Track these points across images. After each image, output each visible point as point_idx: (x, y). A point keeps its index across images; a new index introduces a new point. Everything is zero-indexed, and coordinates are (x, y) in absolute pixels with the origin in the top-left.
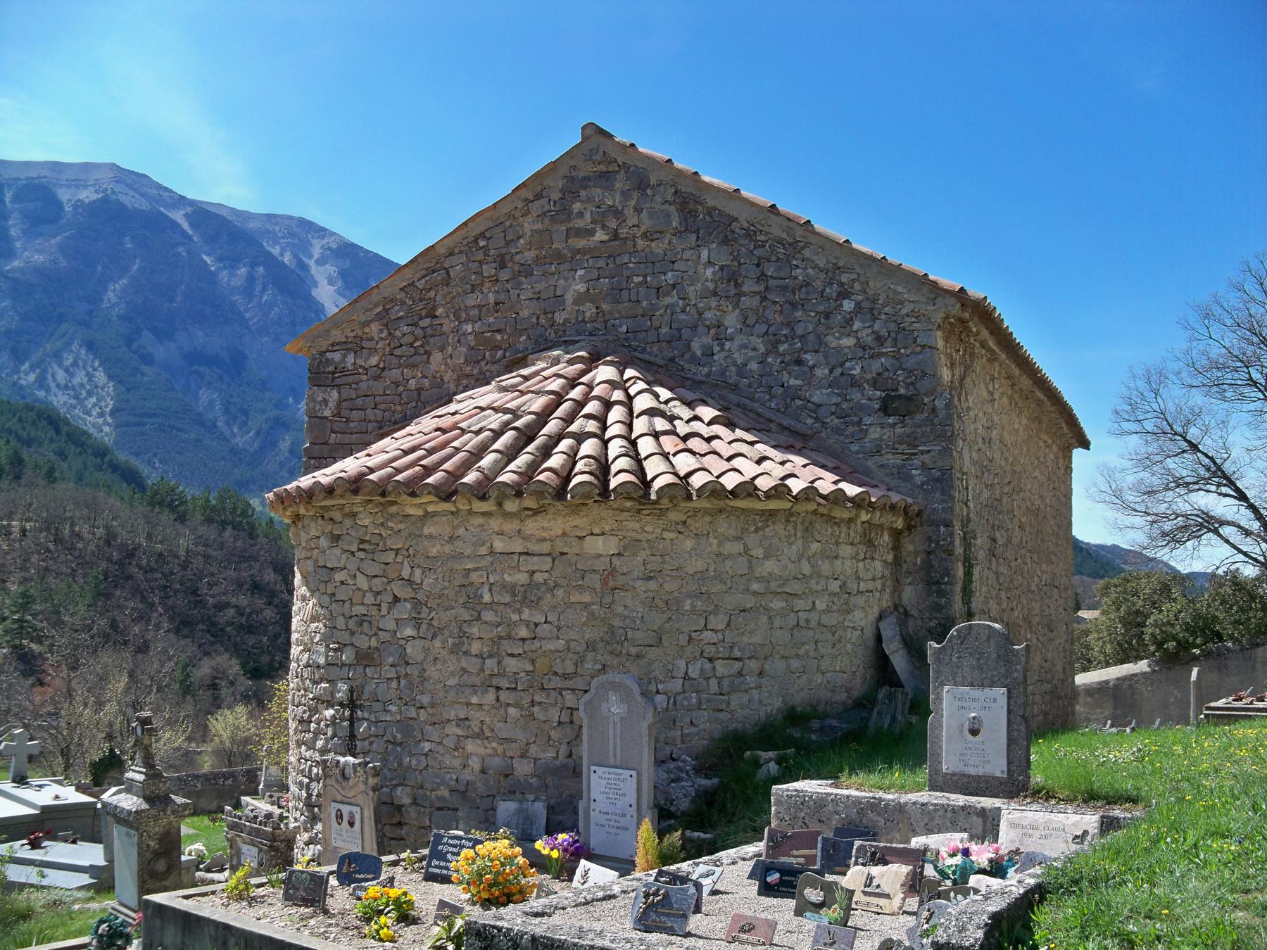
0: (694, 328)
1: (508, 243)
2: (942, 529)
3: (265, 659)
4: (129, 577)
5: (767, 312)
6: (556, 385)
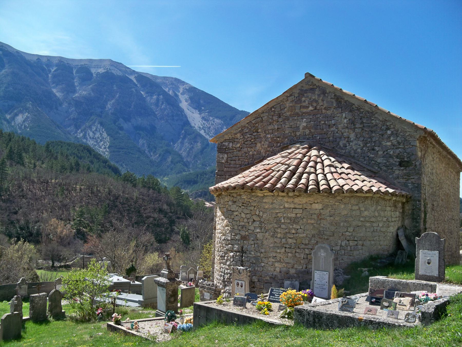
0: (340, 138)
1: (281, 110)
2: (418, 202)
3: (163, 236)
4: (116, 206)
5: (363, 134)
6: (300, 156)
